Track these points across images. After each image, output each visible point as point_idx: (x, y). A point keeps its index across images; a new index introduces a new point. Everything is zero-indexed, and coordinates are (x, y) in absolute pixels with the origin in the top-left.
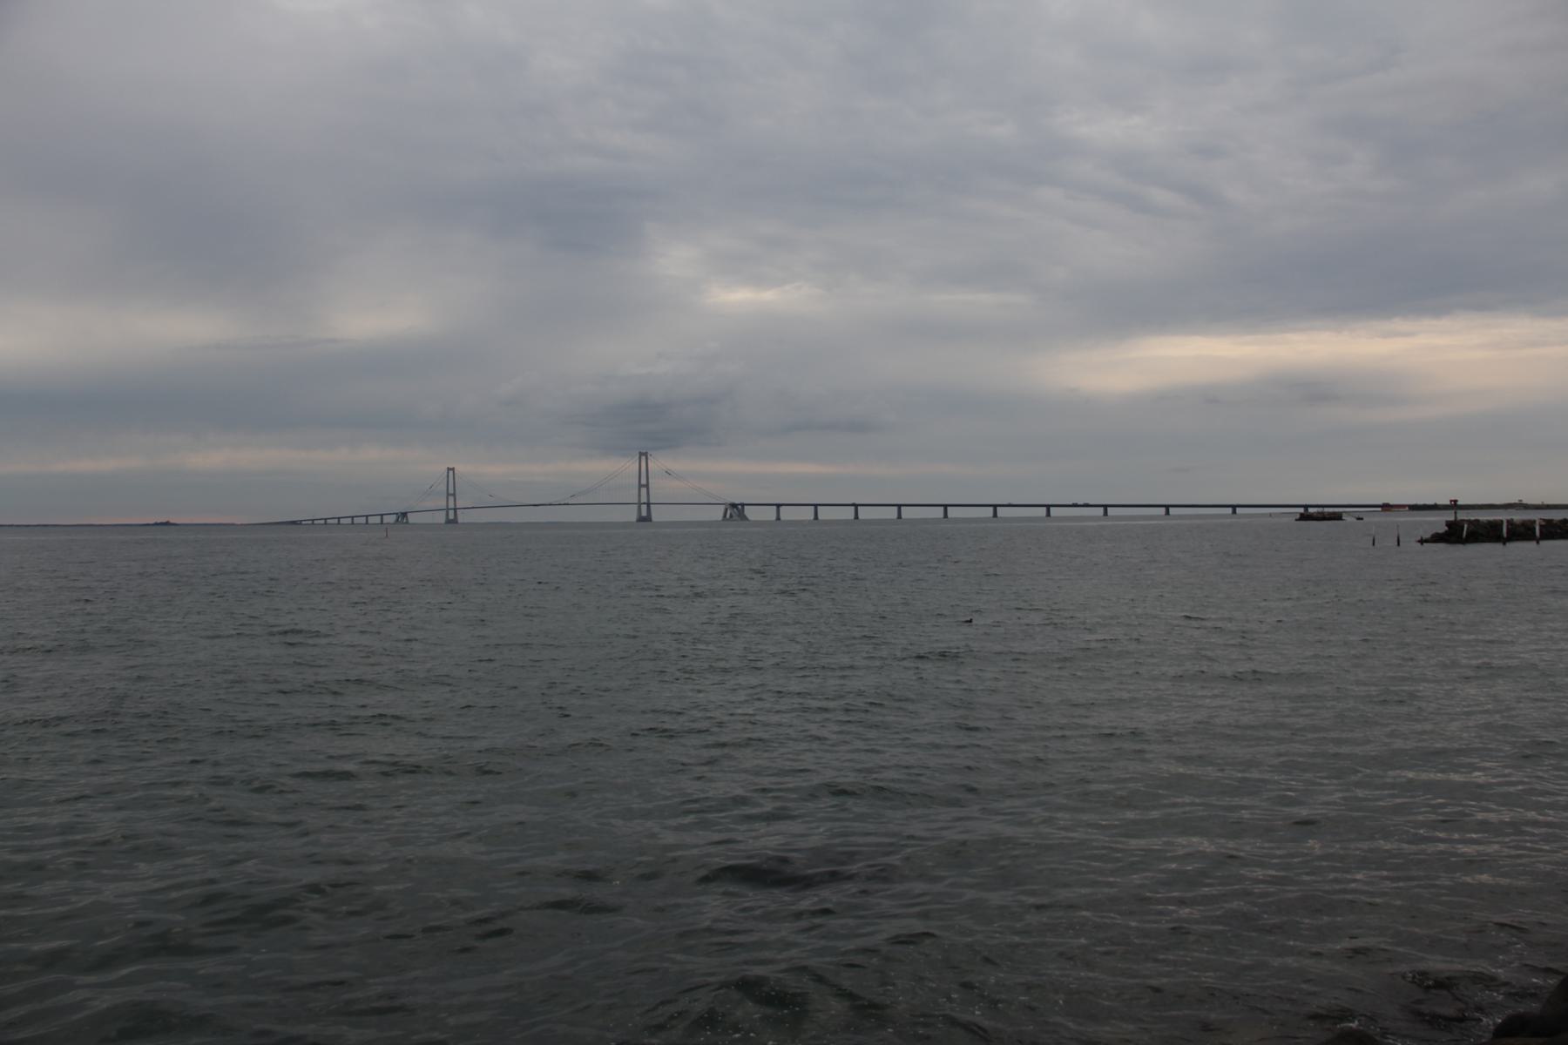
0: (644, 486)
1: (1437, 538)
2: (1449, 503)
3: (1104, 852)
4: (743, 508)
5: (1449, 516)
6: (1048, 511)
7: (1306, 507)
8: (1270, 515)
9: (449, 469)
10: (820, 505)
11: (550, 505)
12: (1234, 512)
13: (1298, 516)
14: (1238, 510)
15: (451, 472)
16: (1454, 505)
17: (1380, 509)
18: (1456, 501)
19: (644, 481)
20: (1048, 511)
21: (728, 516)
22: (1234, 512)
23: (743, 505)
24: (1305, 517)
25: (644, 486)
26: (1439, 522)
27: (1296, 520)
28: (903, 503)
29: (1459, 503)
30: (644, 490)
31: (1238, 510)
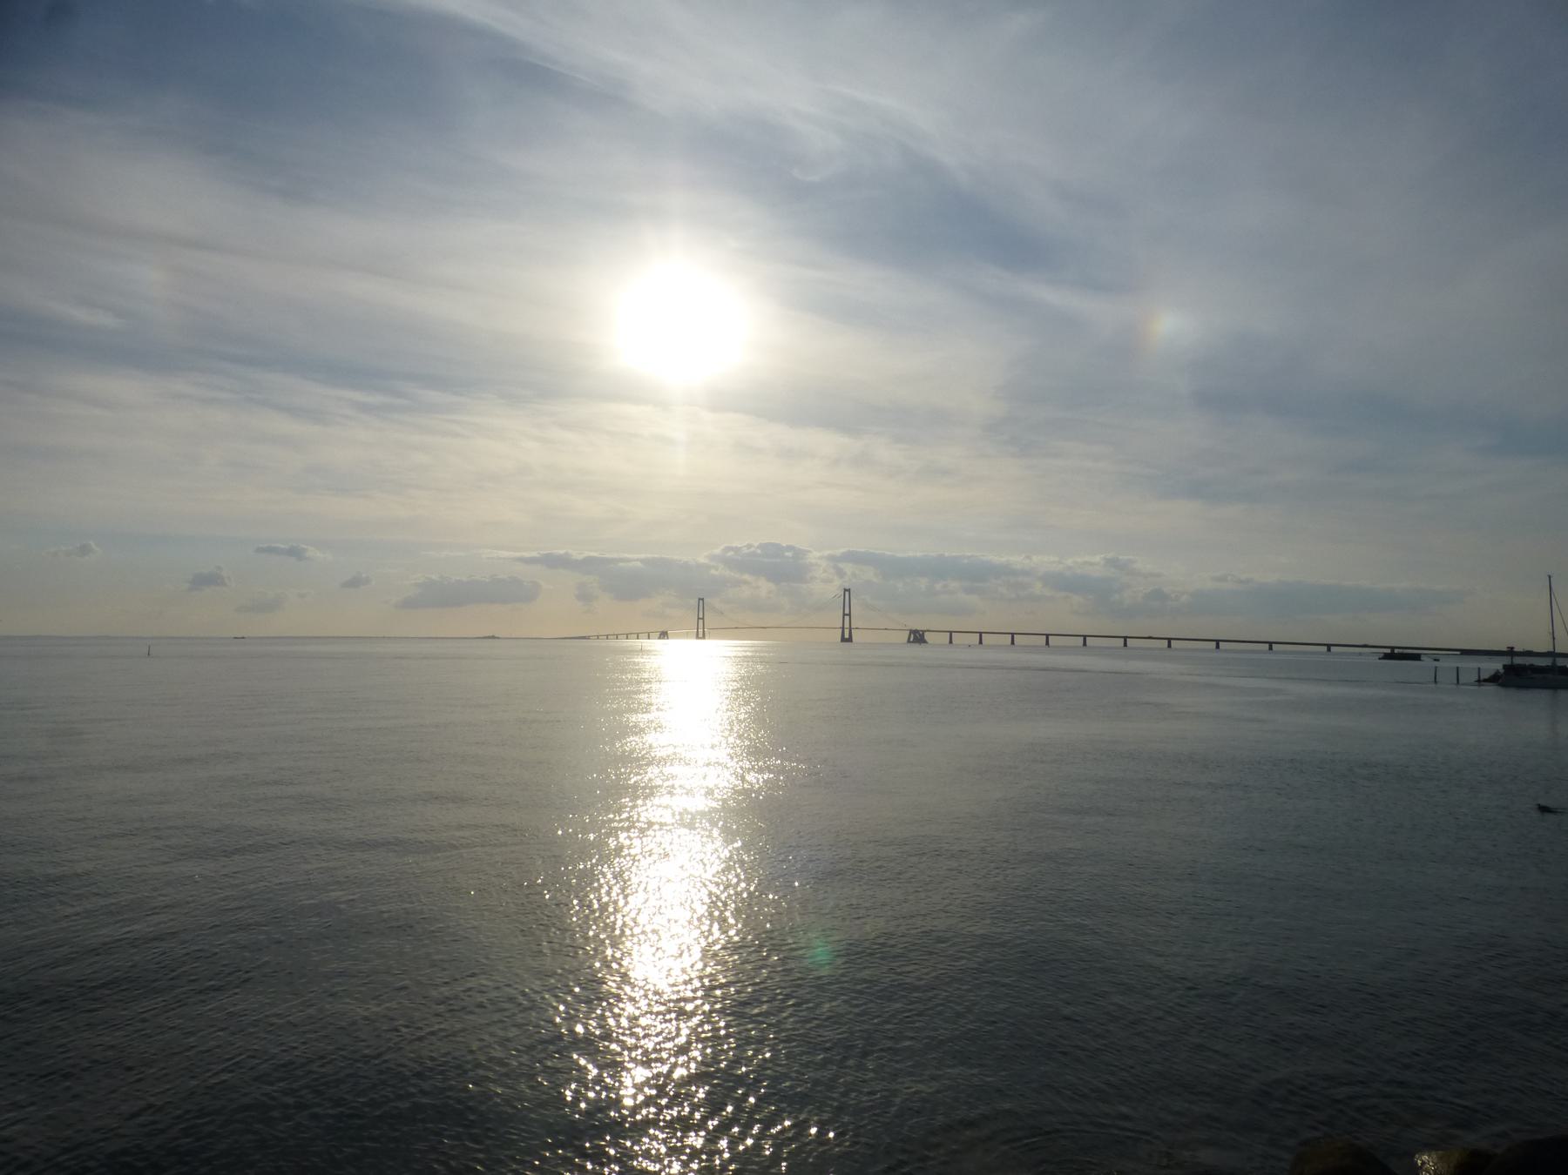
0: (847, 615)
1: (1494, 679)
2: (1505, 649)
3: (870, 1104)
4: (923, 635)
5: (1507, 660)
6: (1125, 641)
7: (1393, 648)
8: (1360, 654)
9: (845, 590)
10: (1051, 635)
11: (1150, 638)
12: (1329, 650)
13: (1382, 655)
14: (1333, 649)
15: (847, 593)
16: (1511, 652)
17: (1458, 653)
18: (1512, 648)
19: (847, 611)
20: (1125, 641)
21: (912, 640)
22: (1329, 650)
23: (924, 631)
24: (1387, 657)
25: (847, 615)
26: (1497, 665)
27: (1380, 659)
28: (928, 628)
29: (1515, 650)
30: (847, 618)
31: (1333, 649)
